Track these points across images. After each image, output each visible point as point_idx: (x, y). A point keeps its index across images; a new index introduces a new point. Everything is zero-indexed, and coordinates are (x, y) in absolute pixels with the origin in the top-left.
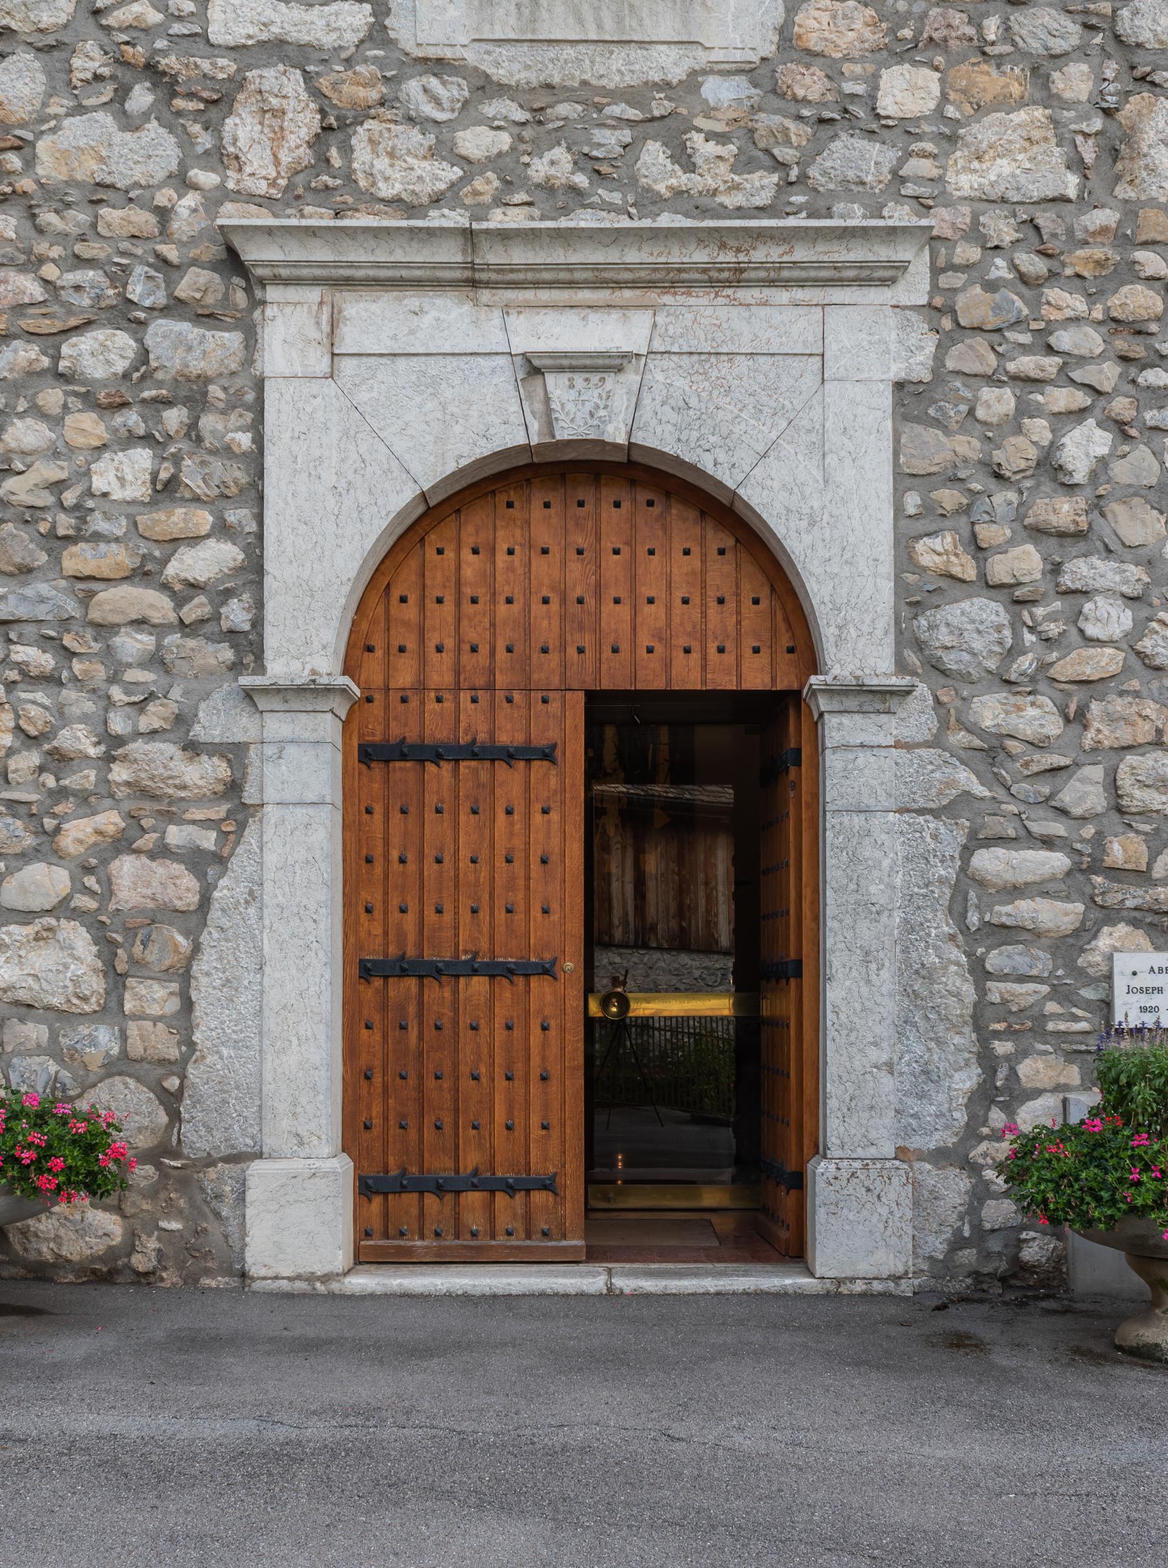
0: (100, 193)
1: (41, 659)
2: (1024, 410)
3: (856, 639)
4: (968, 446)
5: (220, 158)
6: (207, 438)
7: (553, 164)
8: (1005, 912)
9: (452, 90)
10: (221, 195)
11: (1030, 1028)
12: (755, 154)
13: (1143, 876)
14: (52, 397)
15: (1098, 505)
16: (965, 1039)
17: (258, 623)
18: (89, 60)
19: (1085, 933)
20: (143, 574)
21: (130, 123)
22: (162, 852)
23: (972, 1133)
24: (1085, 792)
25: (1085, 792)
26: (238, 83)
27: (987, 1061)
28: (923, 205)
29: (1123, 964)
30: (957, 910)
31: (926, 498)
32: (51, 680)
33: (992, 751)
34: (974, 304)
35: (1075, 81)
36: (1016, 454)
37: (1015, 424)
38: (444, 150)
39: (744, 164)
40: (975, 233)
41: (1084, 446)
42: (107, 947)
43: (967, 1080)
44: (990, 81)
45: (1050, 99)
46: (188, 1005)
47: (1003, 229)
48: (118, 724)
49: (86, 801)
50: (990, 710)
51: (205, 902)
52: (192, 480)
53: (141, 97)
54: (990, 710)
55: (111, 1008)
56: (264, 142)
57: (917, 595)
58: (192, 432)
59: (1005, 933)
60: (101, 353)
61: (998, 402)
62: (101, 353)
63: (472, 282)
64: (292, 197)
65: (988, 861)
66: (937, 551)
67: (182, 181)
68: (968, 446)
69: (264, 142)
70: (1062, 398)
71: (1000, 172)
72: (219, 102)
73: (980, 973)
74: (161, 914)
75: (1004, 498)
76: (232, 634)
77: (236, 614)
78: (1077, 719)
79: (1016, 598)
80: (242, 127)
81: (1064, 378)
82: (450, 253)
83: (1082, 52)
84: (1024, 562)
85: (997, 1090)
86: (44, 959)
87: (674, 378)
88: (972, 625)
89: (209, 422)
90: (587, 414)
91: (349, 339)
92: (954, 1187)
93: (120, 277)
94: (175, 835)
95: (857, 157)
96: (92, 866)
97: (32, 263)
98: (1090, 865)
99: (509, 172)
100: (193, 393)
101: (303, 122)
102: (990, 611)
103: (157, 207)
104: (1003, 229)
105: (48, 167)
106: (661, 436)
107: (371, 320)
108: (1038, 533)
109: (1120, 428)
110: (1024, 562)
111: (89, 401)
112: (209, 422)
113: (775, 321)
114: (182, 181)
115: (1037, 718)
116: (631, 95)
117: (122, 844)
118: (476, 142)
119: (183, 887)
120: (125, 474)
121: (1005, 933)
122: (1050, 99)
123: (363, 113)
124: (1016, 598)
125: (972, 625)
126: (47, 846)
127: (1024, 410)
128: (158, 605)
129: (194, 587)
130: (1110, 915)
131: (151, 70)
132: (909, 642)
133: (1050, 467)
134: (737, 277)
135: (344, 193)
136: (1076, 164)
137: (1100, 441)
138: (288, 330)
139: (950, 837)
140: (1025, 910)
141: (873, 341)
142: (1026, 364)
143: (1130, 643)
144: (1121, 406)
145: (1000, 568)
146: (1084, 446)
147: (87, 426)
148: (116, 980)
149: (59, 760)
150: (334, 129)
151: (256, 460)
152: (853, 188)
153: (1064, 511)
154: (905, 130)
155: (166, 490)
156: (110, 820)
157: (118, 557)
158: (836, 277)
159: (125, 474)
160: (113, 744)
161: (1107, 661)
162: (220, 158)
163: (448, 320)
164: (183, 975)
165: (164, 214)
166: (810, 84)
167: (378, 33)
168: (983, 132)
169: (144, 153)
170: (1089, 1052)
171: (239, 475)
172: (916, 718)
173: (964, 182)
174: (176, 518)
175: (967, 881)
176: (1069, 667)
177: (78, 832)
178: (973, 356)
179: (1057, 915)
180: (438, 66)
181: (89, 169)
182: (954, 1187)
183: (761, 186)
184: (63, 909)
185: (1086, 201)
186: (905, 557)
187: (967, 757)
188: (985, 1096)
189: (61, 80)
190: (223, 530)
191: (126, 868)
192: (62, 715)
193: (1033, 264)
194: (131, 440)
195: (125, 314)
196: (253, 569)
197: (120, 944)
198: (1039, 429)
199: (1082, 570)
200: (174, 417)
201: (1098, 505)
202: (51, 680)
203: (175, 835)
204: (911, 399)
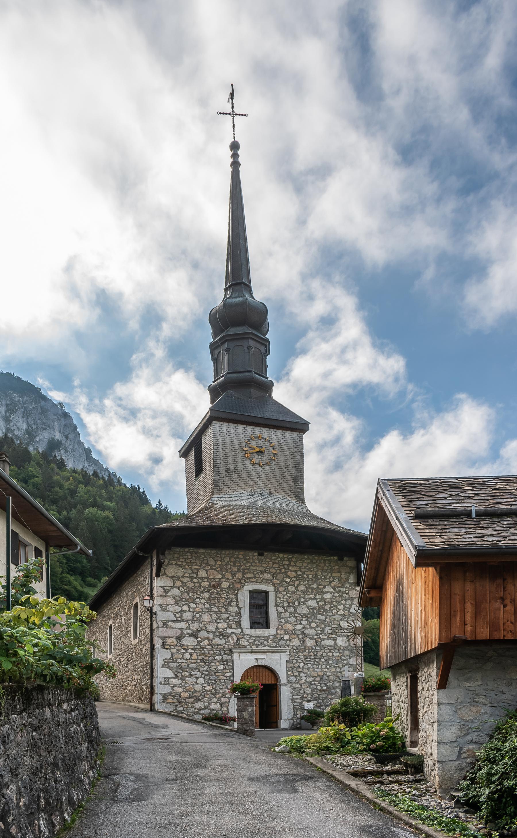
0: (218, 645)
1: (214, 682)
2: (297, 662)
3: (283, 679)
4: (292, 665)
5: (228, 642)
6: (229, 665)
7: (257, 642)
8: (296, 701)
9: (248, 637)
10: (229, 645)
11: (298, 709)
12: (274, 642)
13: (307, 698)
14: (215, 661)
15: (303, 669)
16: (293, 710)
17: (233, 679)
18: (217, 634)
19: (302, 702)
20: (223, 675)
21: (220, 639)
22: (226, 697)
23: (293, 717)
24: (302, 691)
25: (302, 691)
26: (230, 636)
27: (294, 712)
28: (288, 646)
29: (305, 704)
30: (292, 700)
31: (289, 669)
32: (215, 684)
33: (294, 688)
34: (292, 654)
35: (300, 636)
36: (296, 665)
37: (296, 663)
38: (248, 641)
39: (273, 643)
40: (292, 648)
41: (302, 665)
42: (221, 705)
43: (293, 713)
44: (293, 636)
45: (298, 638)
46: (228, 709)
47: (295, 648)
48: (221, 687)
49: (218, 693)
50: (294, 685)
51: (229, 701)
52: (227, 667)
53: (221, 637)
54: (294, 685)
55: (221, 710)
56: (232, 641)
57: (288, 676)
58: (227, 664)
59: (296, 702)
60: (219, 658)
61: (294, 661)
62: (219, 658)
63: (251, 652)
64: (235, 645)
65: (294, 697)
66: (289, 673)
67: (225, 644)
68: (292, 665)
69: (232, 641)
70: (300, 661)
71: (294, 643)
72: (228, 637)
73: (294, 705)
74: (225, 702)
75: (295, 669)
76: (231, 680)
77: (231, 678)
78: (301, 686)
79: (296, 677)
80: (230, 639)
81: (300, 659)
82: (250, 650)
83: (301, 634)
84: (297, 674)
85: (295, 714)
86: (215, 706)
87: (266, 659)
88: (293, 679)
89: (229, 663)
90: (261, 663)
91: (241, 657)
92: (292, 721)
93: (220, 652)
94: (226, 696)
95: (282, 642)
96: (219, 699)
97: (213, 650)
98: (302, 697)
99: (253, 643)
100: (227, 661)
101: (236, 639)
102: (294, 678)
103: (366, 616)
104: (295, 648)
105: (213, 642)
106: (267, 664)
107: (243, 655)
108: (298, 671)
109: (304, 664)
110: (297, 674)
111: (218, 662)
112: (229, 663)
113: (276, 655)
114: (225, 644)
115: (298, 686)
116: (263, 637)
117: (222, 697)
118: (251, 641)
119: (228, 700)
120: (221, 667)
121: (296, 702)
122: (298, 638)
123: (241, 638)
124: (296, 677)
125: (293, 679)
126: (215, 697)
127: (297, 662)
128: (225, 678)
129: (228, 676)
130: (304, 701)
131: (222, 635)
132: (288, 681)
133: (299, 667)
134: (274, 652)
135: (240, 645)
136: (301, 643)
137: (303, 665)
138: (235, 656)
139: (291, 695)
140: (297, 700)
141: (284, 657)
142: (297, 658)
143: (305, 680)
144: (305, 662)
145: (295, 674)
146: (302, 665)
147: (218, 663)
148: (222, 707)
149: (216, 690)
150: (238, 640)
151: (233, 666)
152: (282, 645)
153: (300, 670)
154: (286, 640)
155: (225, 669)
156: (221, 695)
157: (221, 674)
158: (282, 652)
159: (221, 667)
160: (221, 689)
161: (304, 681)
162: (228, 642)
163: (249, 655)
164: (228, 707)
165: (224, 647)
166: (279, 636)
167: (242, 632)
168: (293, 640)
169: (222, 641)
170: (351, 629)
171: (231, 667)
172: (288, 686)
173: (291, 644)
174: (226, 671)
175: (293, 698)
176: (301, 682)
177: (218, 696)
178: (292, 658)
179: (300, 701)
180: (247, 635)
181: (217, 643)
182: (292, 721)
183: (275, 644)
184: (217, 702)
185: (301, 646)
186: (287, 673)
187: (292, 689)
188: (294, 715)
189: (214, 635)
190: (230, 672)
191: (222, 699)
192: (216, 687)
193: (297, 651)
194: (222, 665)
195: (220, 654)
196: (233, 675)
197: (222, 704)
198: (298, 663)
199: (301, 674)
200: (225, 663)
201: (303, 669)
202: (215, 684)
203: (226, 696)
204: (288, 661)
